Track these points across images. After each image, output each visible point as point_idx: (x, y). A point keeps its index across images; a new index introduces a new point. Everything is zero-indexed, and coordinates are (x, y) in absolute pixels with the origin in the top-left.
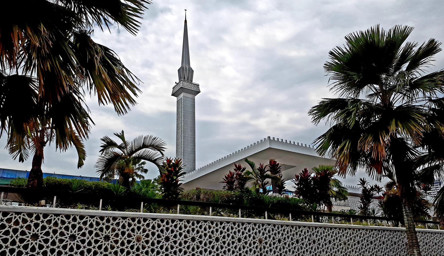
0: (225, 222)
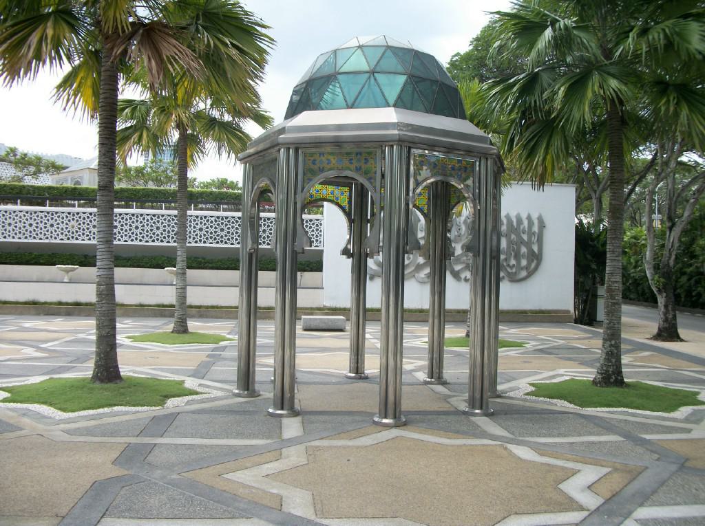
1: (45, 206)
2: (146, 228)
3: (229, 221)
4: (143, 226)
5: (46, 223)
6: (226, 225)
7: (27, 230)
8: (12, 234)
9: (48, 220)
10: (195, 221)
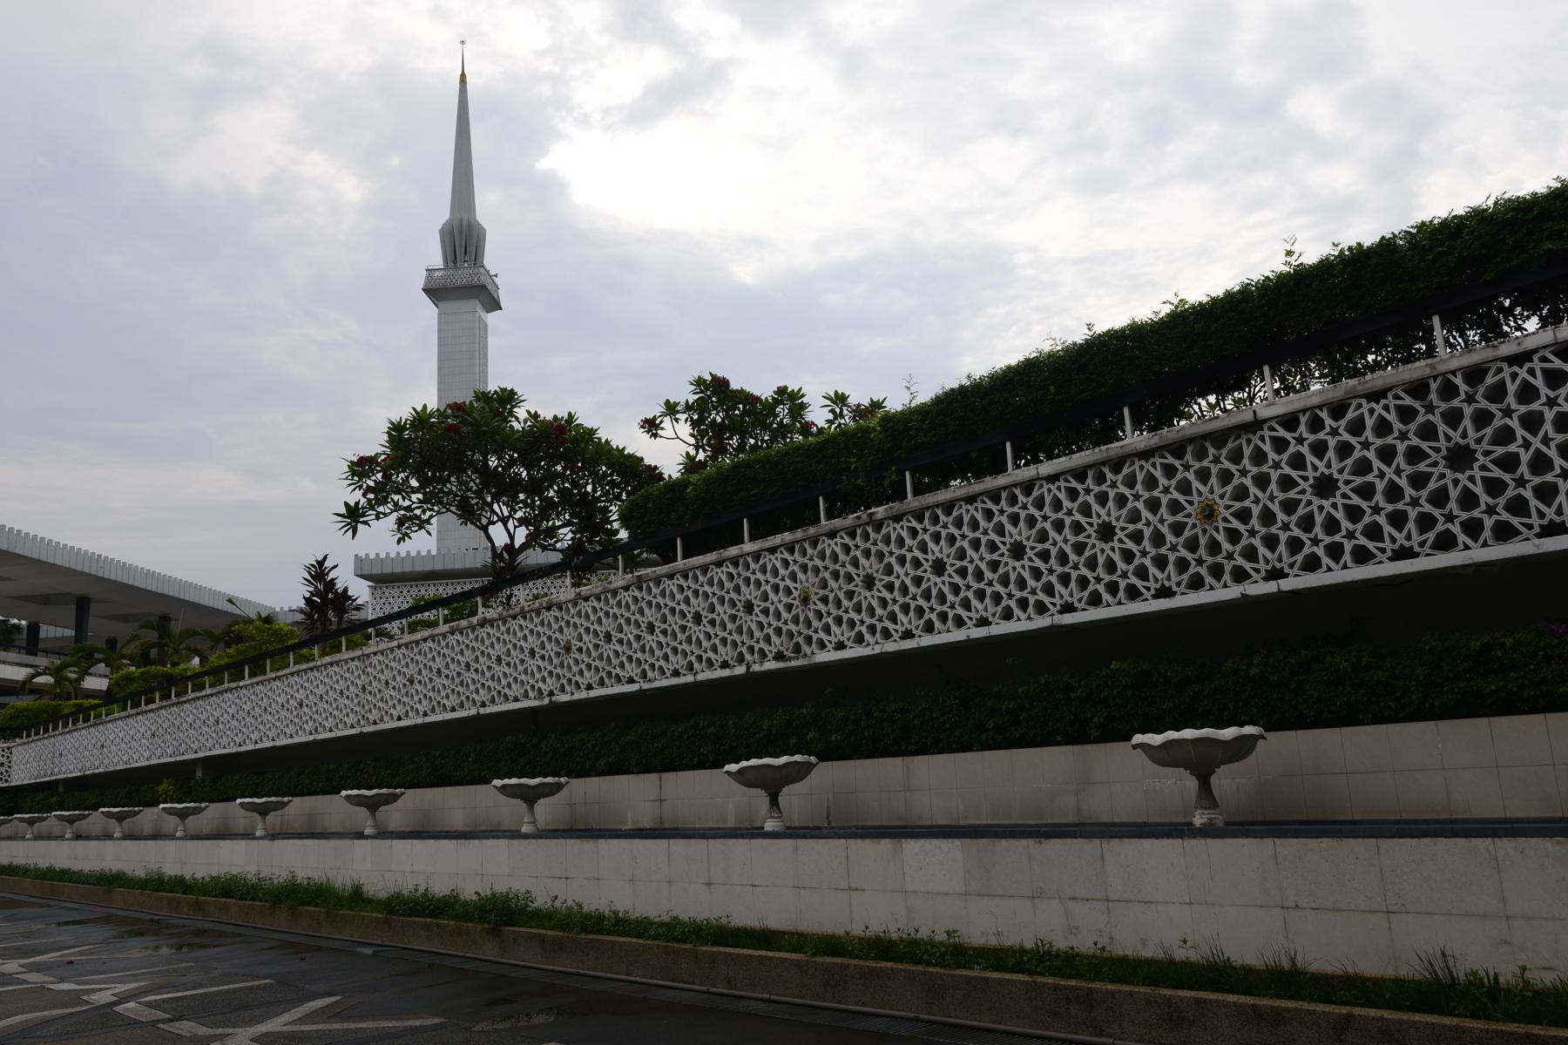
0: (1354, 403)
1: (264, 673)
2: (1381, 475)
3: (1497, 394)
4: (1363, 467)
5: (1287, 483)
6: (1482, 419)
7: (1092, 564)
8: (1351, 535)
9: (1319, 449)
10: (1280, 445)
